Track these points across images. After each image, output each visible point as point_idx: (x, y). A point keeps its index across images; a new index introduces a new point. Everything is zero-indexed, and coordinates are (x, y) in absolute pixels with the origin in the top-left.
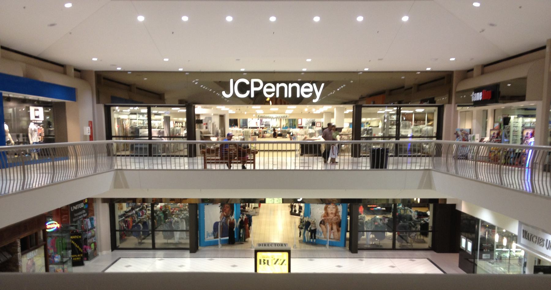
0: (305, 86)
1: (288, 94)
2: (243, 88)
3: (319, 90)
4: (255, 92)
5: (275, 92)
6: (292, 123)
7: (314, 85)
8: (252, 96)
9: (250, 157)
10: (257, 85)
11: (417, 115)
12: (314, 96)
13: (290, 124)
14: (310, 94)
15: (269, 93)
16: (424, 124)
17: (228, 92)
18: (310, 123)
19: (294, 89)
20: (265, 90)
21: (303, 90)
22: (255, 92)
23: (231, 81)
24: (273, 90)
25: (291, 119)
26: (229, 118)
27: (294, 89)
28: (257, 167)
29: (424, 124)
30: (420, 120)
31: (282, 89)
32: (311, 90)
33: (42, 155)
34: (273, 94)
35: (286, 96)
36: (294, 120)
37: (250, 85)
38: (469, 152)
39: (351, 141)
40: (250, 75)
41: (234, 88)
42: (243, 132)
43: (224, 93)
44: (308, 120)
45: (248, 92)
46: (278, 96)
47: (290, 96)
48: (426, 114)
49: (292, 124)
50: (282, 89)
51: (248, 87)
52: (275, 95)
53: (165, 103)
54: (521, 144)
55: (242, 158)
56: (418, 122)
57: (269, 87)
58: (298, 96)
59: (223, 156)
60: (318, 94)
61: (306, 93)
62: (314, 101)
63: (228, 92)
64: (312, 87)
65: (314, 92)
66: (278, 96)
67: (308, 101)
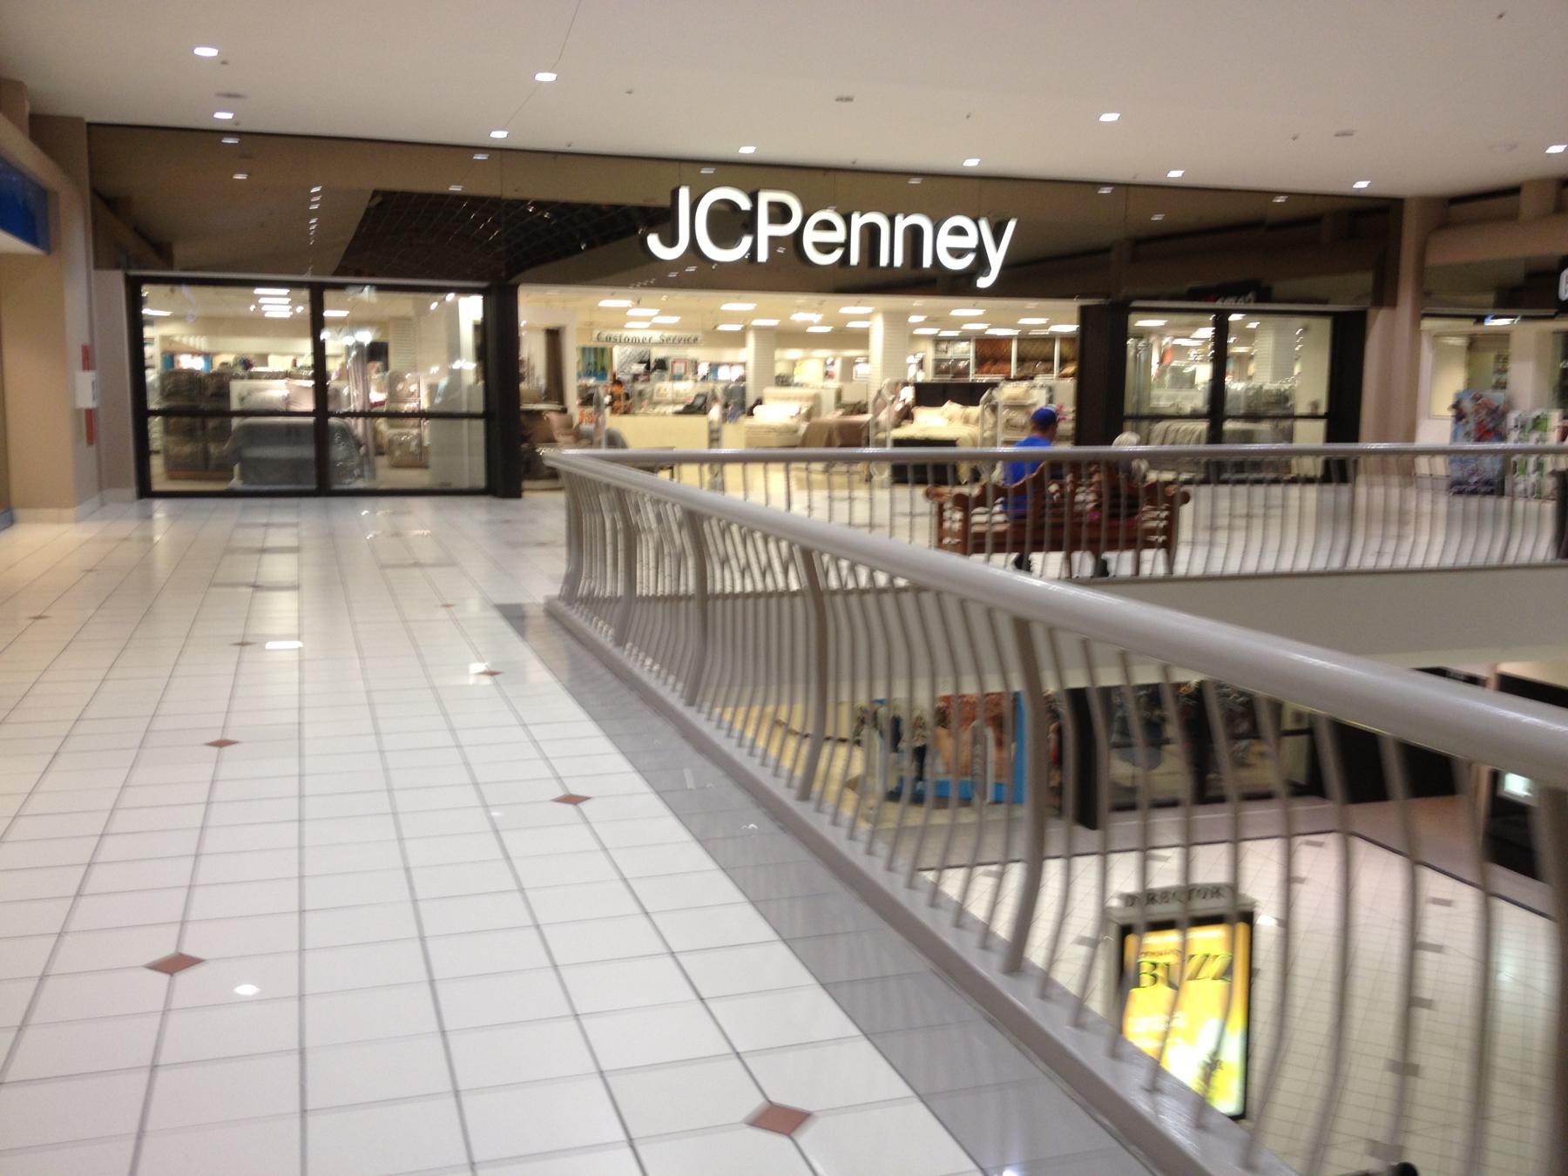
0: (817, 221)
1: (892, 253)
2: (730, 224)
3: (997, 238)
4: (774, 241)
5: (846, 245)
6: (592, 360)
7: (983, 224)
8: (763, 256)
9: (1152, 518)
10: (780, 213)
11: (1024, 344)
12: (982, 264)
13: (589, 364)
14: (970, 258)
15: (825, 248)
16: (1050, 371)
17: (670, 240)
18: (631, 360)
19: (915, 234)
20: (811, 236)
21: (946, 241)
22: (774, 241)
23: (684, 195)
24: (838, 236)
25: (590, 349)
26: (577, 345)
27: (915, 234)
28: (1180, 569)
29: (1050, 371)
30: (1035, 359)
31: (872, 232)
32: (970, 242)
33: (1385, 522)
34: (838, 253)
35: (884, 261)
36: (599, 352)
37: (754, 212)
38: (1068, 489)
39: (1203, 447)
40: (754, 173)
41: (693, 220)
42: (625, 406)
43: (653, 242)
44: (624, 353)
45: (747, 241)
46: (854, 259)
47: (898, 262)
48: (1054, 340)
49: (596, 363)
50: (872, 232)
51: (748, 223)
52: (845, 258)
53: (171, 267)
54: (710, 446)
55: (1122, 522)
56: (1026, 365)
57: (827, 226)
58: (927, 262)
59: (1043, 516)
60: (996, 258)
61: (958, 253)
62: (984, 282)
63: (670, 240)
64: (975, 232)
65: (980, 250)
66: (854, 259)
67: (960, 285)
